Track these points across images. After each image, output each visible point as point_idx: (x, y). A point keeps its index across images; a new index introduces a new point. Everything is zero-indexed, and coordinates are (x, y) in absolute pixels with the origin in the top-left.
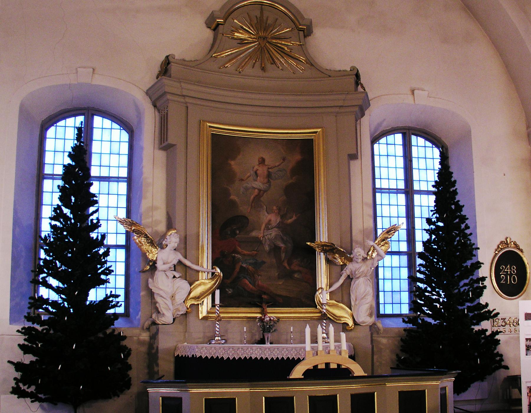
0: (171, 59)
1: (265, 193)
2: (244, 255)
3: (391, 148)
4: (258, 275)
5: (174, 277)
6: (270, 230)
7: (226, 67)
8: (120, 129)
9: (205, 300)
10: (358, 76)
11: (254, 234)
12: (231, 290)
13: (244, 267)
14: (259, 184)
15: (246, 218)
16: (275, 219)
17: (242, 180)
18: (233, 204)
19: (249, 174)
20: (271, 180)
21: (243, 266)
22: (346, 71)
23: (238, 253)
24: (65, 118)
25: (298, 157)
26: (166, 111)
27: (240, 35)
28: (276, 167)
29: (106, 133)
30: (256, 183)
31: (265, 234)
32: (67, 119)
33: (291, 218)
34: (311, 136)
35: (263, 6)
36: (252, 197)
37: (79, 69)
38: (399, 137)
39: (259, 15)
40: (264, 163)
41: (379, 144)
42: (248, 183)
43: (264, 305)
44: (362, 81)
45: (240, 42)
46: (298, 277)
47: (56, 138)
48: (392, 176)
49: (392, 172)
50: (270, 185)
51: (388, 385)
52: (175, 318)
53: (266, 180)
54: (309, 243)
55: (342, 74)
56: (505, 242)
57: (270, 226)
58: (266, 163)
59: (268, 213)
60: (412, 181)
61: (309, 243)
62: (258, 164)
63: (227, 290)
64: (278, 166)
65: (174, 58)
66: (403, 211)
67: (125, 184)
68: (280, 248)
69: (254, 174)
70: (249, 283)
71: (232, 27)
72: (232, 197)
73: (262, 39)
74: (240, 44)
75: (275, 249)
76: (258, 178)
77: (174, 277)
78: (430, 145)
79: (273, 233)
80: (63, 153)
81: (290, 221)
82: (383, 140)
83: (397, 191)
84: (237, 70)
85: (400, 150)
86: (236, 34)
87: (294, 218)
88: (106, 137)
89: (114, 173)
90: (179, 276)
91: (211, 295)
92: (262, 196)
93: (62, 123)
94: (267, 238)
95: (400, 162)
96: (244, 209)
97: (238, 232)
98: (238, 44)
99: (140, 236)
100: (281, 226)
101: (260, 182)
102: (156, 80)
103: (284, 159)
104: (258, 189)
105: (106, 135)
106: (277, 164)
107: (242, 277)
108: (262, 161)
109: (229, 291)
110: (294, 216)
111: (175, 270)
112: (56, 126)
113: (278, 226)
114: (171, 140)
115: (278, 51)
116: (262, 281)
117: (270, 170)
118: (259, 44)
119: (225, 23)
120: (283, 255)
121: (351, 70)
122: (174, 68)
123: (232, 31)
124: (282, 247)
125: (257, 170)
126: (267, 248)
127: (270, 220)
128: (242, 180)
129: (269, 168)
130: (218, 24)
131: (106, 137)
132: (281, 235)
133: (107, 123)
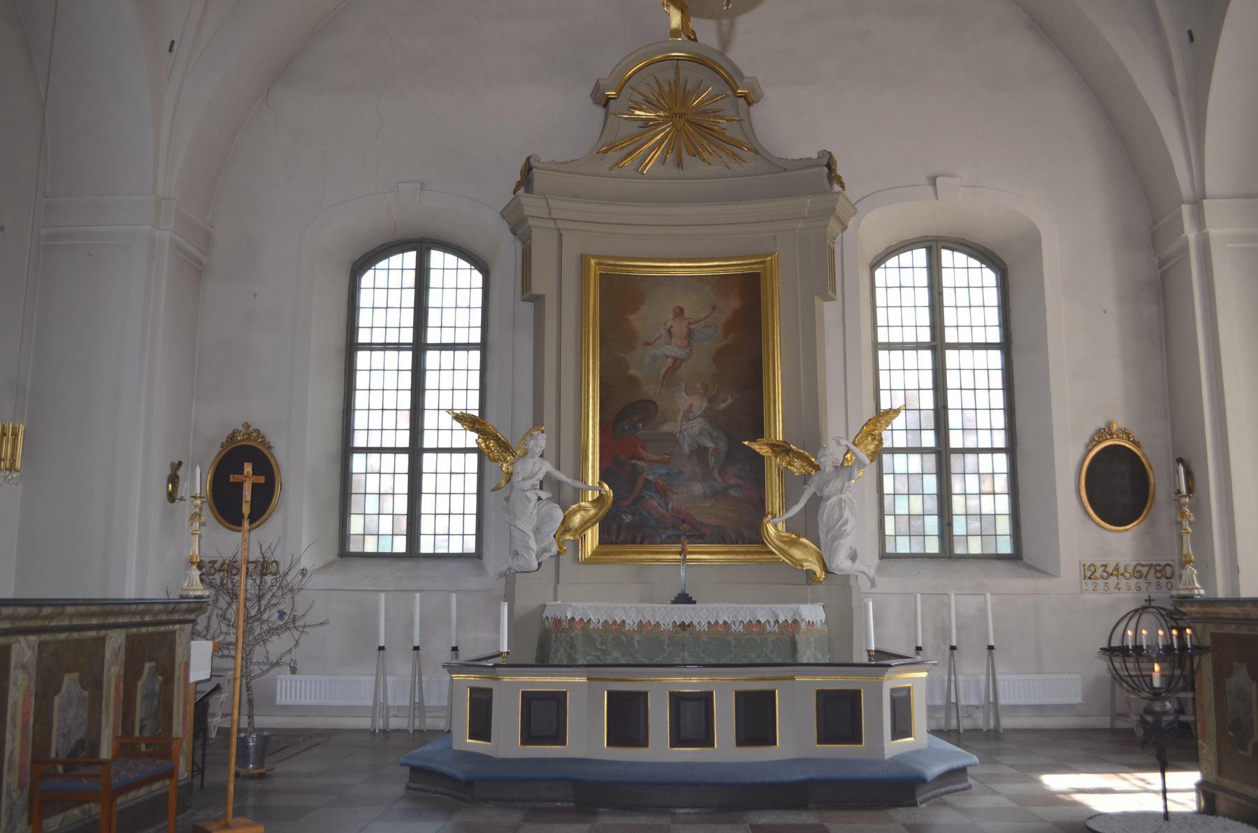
0: (533, 162)
1: (684, 364)
2: (650, 461)
3: (906, 273)
4: (673, 493)
5: (539, 499)
6: (690, 420)
7: (621, 167)
8: (471, 269)
9: (590, 532)
10: (830, 165)
11: (666, 428)
12: (629, 516)
13: (651, 481)
14: (674, 350)
15: (654, 403)
16: (698, 404)
17: (647, 344)
18: (633, 382)
19: (658, 334)
20: (692, 342)
21: (648, 480)
22: (810, 159)
23: (641, 459)
24: (387, 256)
25: (735, 303)
26: (528, 244)
27: (643, 113)
28: (700, 320)
29: (450, 275)
30: (670, 347)
31: (684, 428)
32: (391, 258)
33: (724, 401)
34: (757, 269)
35: (680, 61)
36: (663, 371)
37: (401, 186)
38: (920, 255)
39: (672, 77)
40: (683, 316)
41: (885, 268)
42: (656, 349)
43: (683, 538)
44: (840, 170)
45: (642, 125)
46: (736, 495)
47: (374, 288)
48: (909, 320)
49: (908, 313)
50: (691, 351)
51: (506, 679)
52: (541, 562)
53: (685, 342)
54: (746, 443)
55: (807, 164)
56: (1107, 430)
57: (691, 416)
58: (686, 315)
59: (688, 395)
60: (942, 327)
61: (746, 443)
62: (672, 317)
63: (623, 516)
64: (706, 318)
65: (539, 161)
66: (927, 380)
67: (478, 353)
68: (706, 449)
69: (667, 334)
70: (658, 505)
71: (631, 101)
72: (631, 372)
73: (678, 115)
74: (643, 127)
75: (701, 452)
76: (673, 339)
77: (539, 499)
78: (977, 264)
79: (696, 426)
80: (384, 310)
81: (723, 406)
82: (892, 262)
83: (917, 346)
84: (638, 171)
85: (922, 277)
86: (637, 112)
87: (730, 401)
88: (450, 282)
89: (462, 338)
90: (547, 497)
91: (598, 524)
92: (678, 368)
93: (383, 264)
94: (686, 434)
95: (923, 297)
96: (650, 390)
97: (641, 425)
98: (640, 127)
99: (487, 438)
100: (711, 416)
101: (676, 346)
102: (513, 196)
103: (714, 308)
104: (673, 358)
105: (450, 277)
106: (703, 316)
107: (647, 497)
108: (679, 313)
109: (628, 518)
110: (730, 398)
111: (541, 488)
112: (375, 269)
113: (705, 415)
114: (536, 289)
115: (701, 133)
116: (678, 500)
117: (692, 326)
118: (674, 125)
119: (619, 96)
120: (712, 460)
121: (819, 157)
122: (537, 175)
123: (632, 108)
124: (710, 447)
125: (672, 327)
126: (686, 450)
127: (691, 406)
128: (647, 344)
129: (689, 324)
130: (608, 99)
131: (450, 282)
132: (709, 428)
133: (451, 260)
